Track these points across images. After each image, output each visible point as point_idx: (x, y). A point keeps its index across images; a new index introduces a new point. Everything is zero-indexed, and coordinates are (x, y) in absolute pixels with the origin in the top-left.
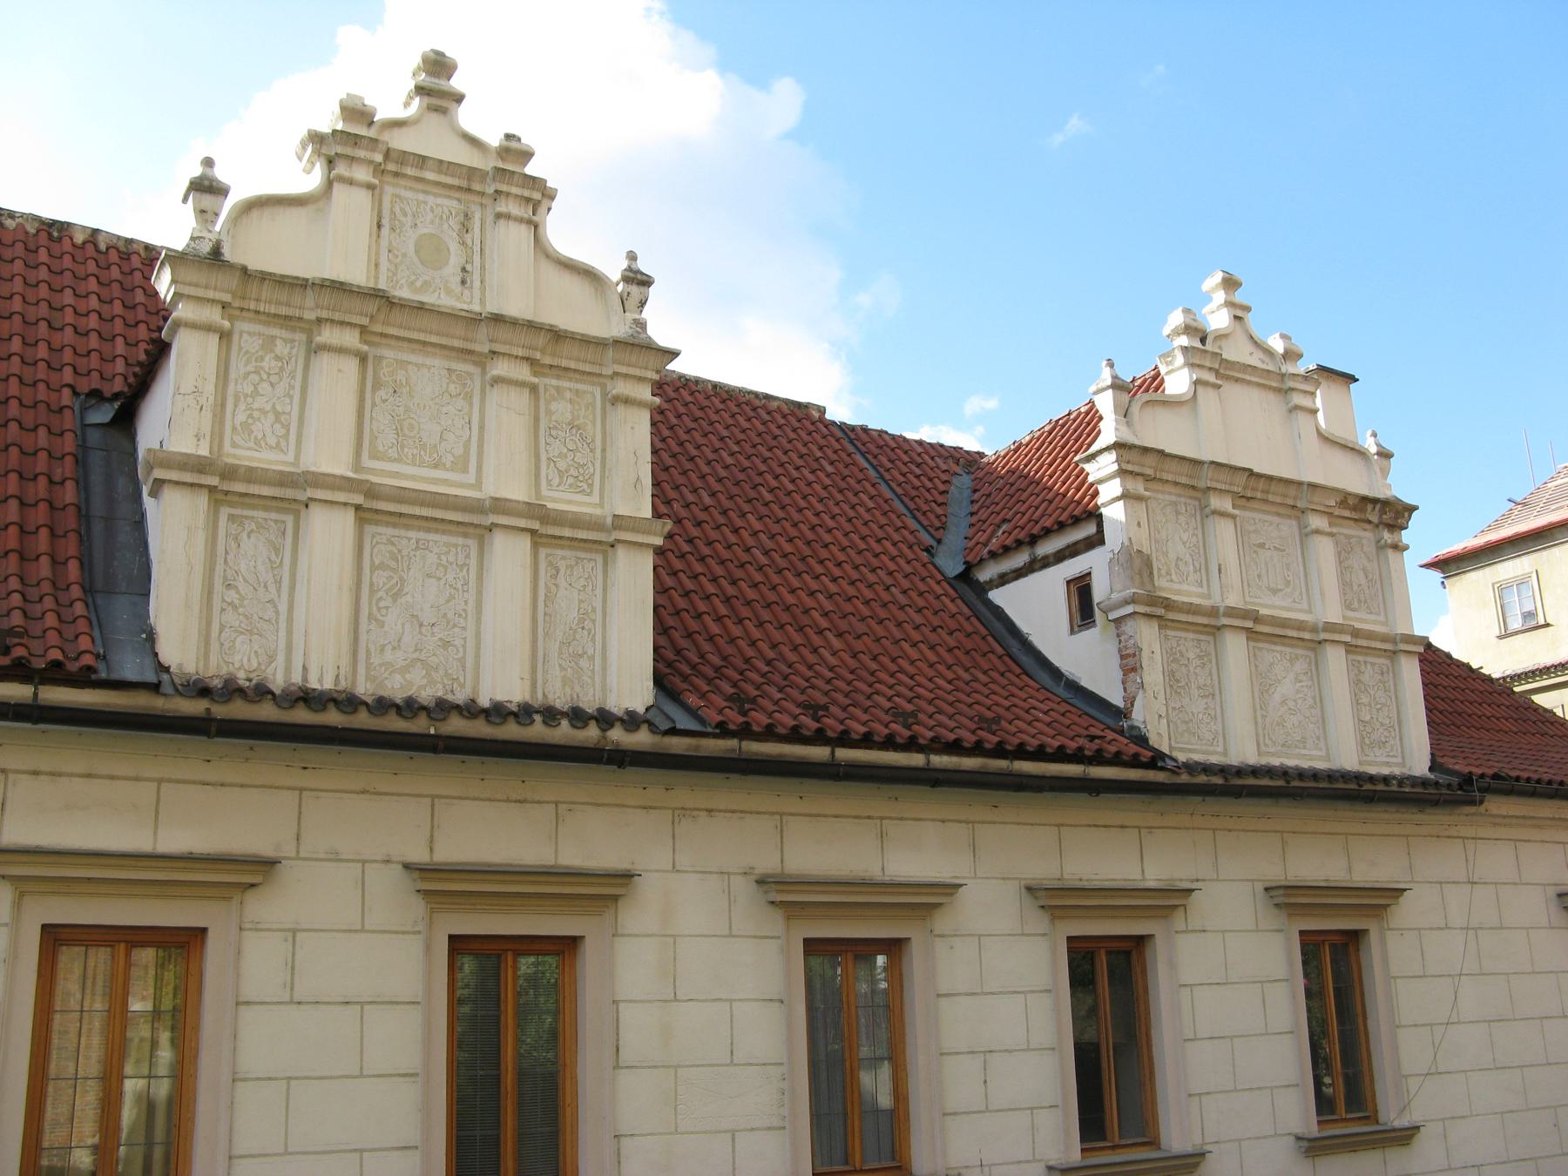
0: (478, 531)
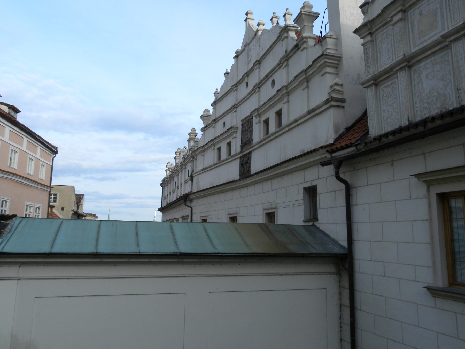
0: (395, 76)
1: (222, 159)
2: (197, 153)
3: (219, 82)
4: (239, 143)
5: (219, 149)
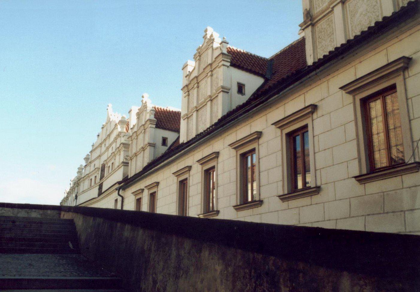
1: (92, 186)
2: (80, 181)
3: (94, 140)
4: (99, 178)
5: (91, 179)
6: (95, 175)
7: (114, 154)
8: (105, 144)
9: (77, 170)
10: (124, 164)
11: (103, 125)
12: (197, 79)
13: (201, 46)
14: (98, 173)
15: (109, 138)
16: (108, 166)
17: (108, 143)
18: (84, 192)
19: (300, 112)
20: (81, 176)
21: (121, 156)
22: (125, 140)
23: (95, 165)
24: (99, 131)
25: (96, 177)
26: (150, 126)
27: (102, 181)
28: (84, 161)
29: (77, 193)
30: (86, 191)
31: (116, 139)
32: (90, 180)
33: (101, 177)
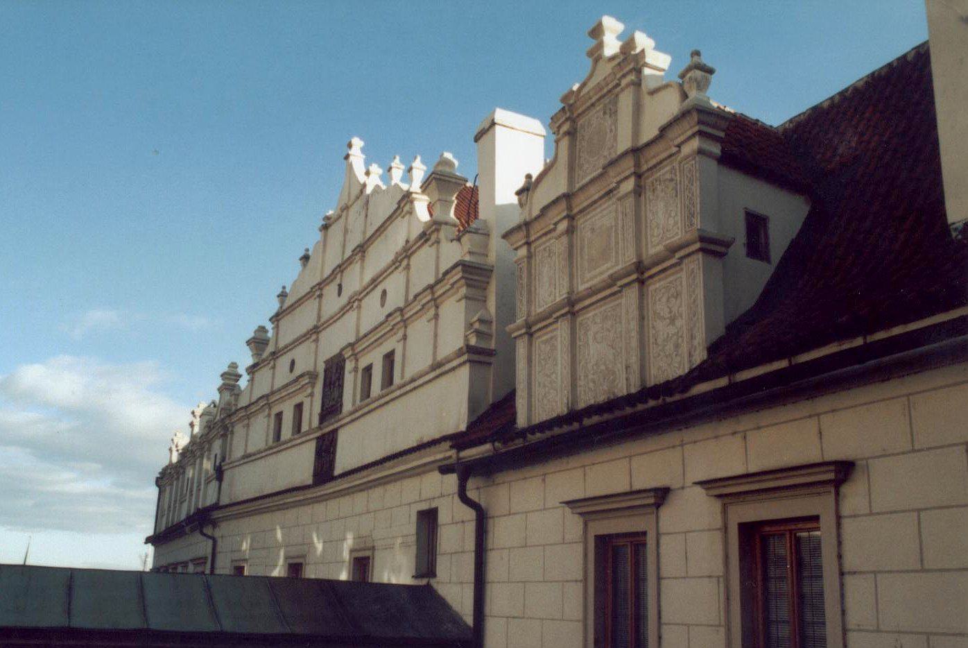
2: (234, 418)
3: (289, 274)
4: (317, 408)
6: (297, 400)
7: (400, 319)
8: (340, 286)
9: (220, 382)
10: (706, 246)
11: (328, 218)
12: (528, 231)
13: (575, 88)
14: (309, 391)
15: (363, 258)
16: (363, 363)
17: (354, 280)
18: (248, 457)
19: (590, 503)
20: (236, 400)
21: (315, 399)
22: (470, 253)
23: (293, 363)
24: (313, 237)
25: (299, 408)
26: (695, 143)
27: (335, 426)
28: (247, 348)
29: (223, 459)
30: (258, 456)
31: (408, 257)
32: (273, 417)
33: (322, 410)
